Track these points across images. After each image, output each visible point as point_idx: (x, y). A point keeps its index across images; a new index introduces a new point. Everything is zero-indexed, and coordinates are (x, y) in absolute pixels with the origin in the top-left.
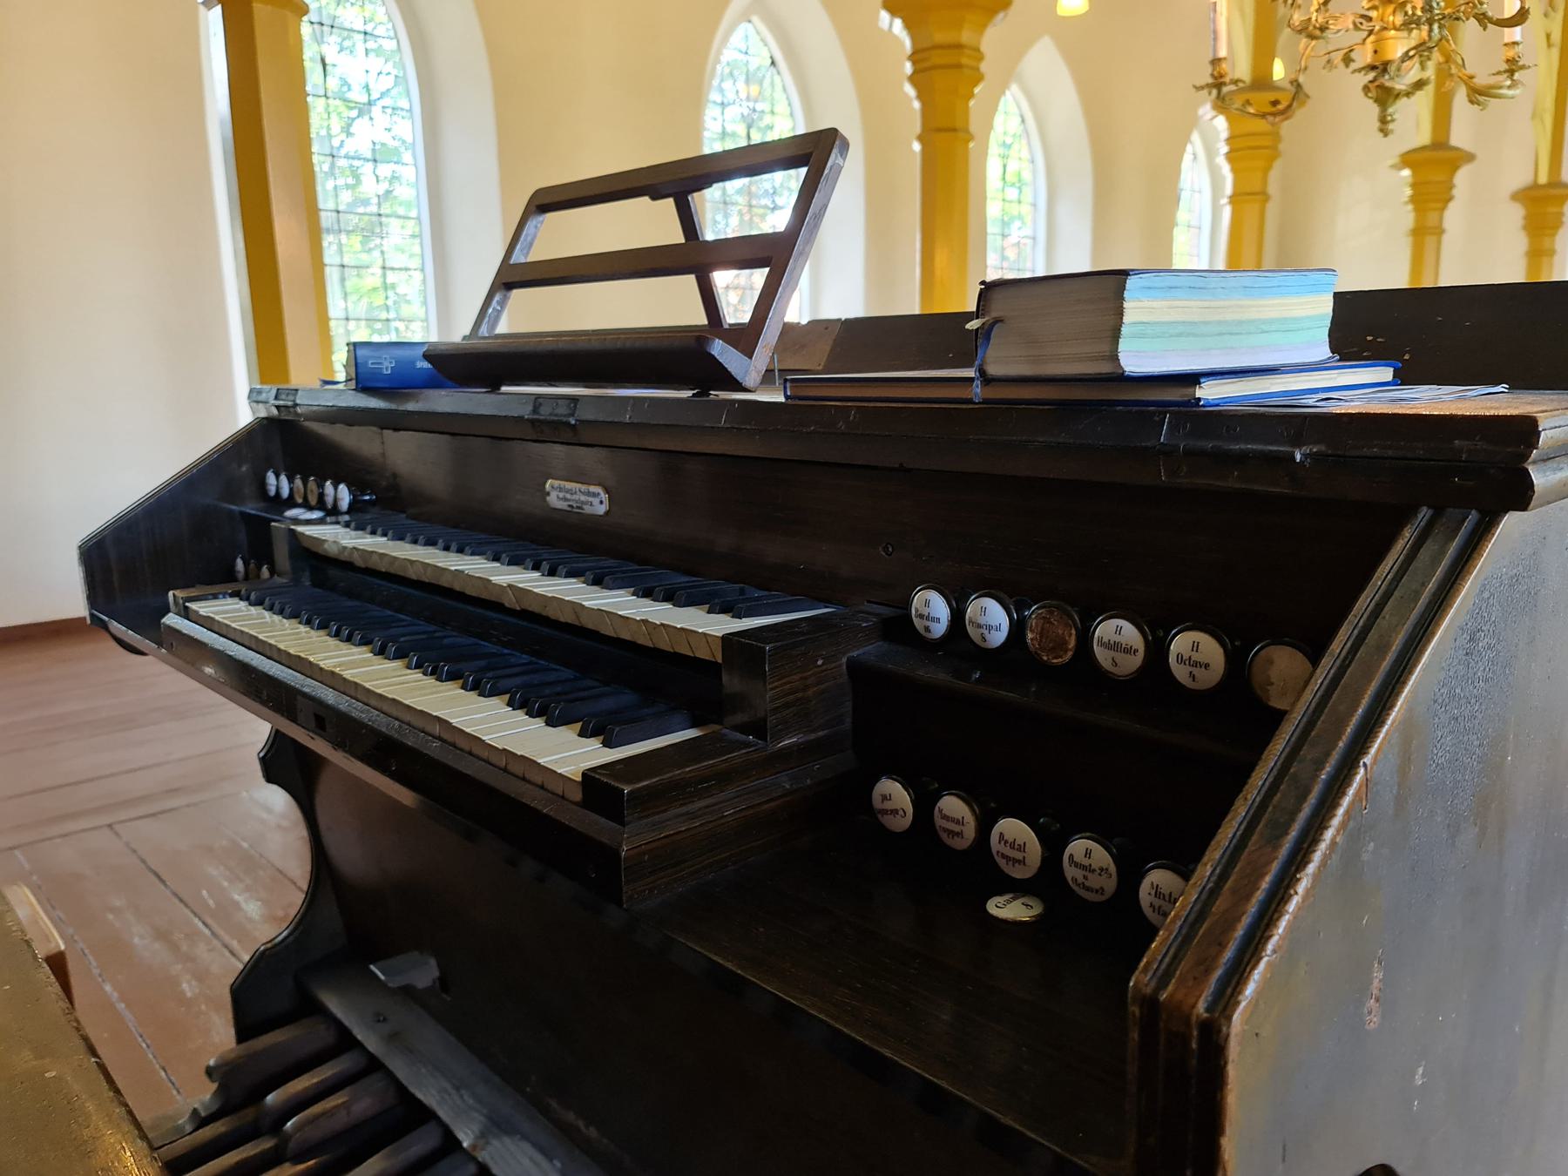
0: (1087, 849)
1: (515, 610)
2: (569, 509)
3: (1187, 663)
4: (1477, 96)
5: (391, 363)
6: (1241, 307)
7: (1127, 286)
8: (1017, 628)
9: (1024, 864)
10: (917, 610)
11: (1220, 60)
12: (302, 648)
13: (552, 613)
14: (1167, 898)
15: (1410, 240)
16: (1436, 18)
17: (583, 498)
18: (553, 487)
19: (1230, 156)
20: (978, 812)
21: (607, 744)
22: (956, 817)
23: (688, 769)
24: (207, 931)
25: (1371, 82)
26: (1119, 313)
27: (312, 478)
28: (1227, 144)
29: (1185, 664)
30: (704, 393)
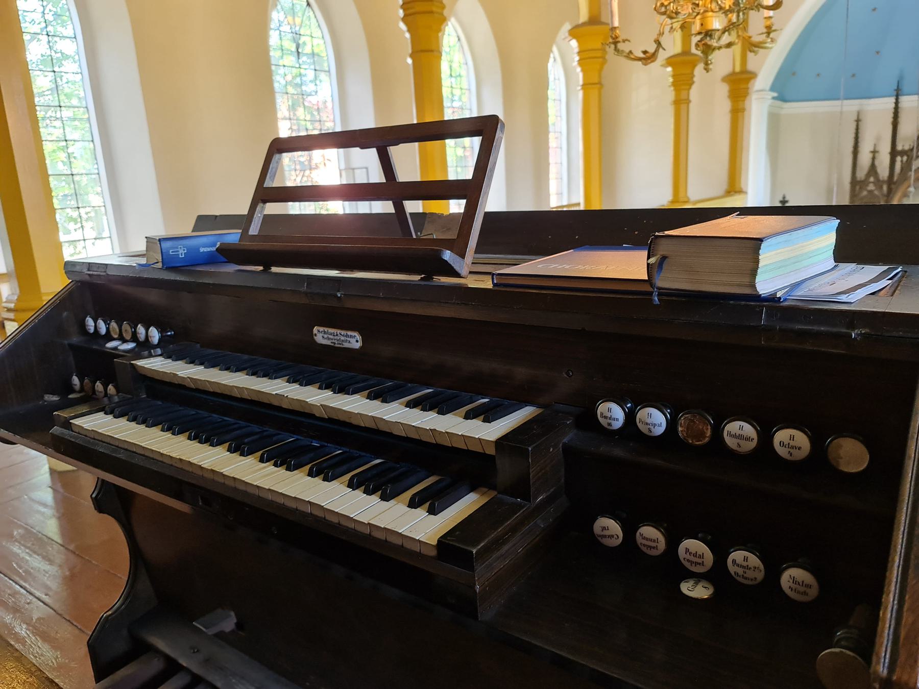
0: (745, 557)
1: (325, 419)
2: (332, 344)
3: (787, 446)
4: (754, 48)
5: (184, 250)
6: (802, 247)
7: (762, 247)
8: (672, 424)
9: (703, 565)
10: (602, 414)
11: (615, 28)
12: (177, 454)
13: (355, 422)
14: (801, 584)
15: (673, 106)
16: (742, 9)
17: (343, 338)
18: (319, 331)
19: (580, 62)
20: (664, 532)
21: (432, 511)
22: (653, 538)
23: (499, 530)
24: (22, 591)
25: (699, 41)
26: (757, 261)
27: (125, 323)
28: (578, 55)
29: (785, 447)
30: (429, 278)
